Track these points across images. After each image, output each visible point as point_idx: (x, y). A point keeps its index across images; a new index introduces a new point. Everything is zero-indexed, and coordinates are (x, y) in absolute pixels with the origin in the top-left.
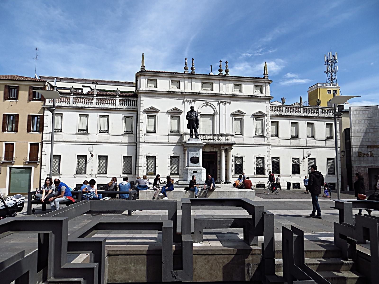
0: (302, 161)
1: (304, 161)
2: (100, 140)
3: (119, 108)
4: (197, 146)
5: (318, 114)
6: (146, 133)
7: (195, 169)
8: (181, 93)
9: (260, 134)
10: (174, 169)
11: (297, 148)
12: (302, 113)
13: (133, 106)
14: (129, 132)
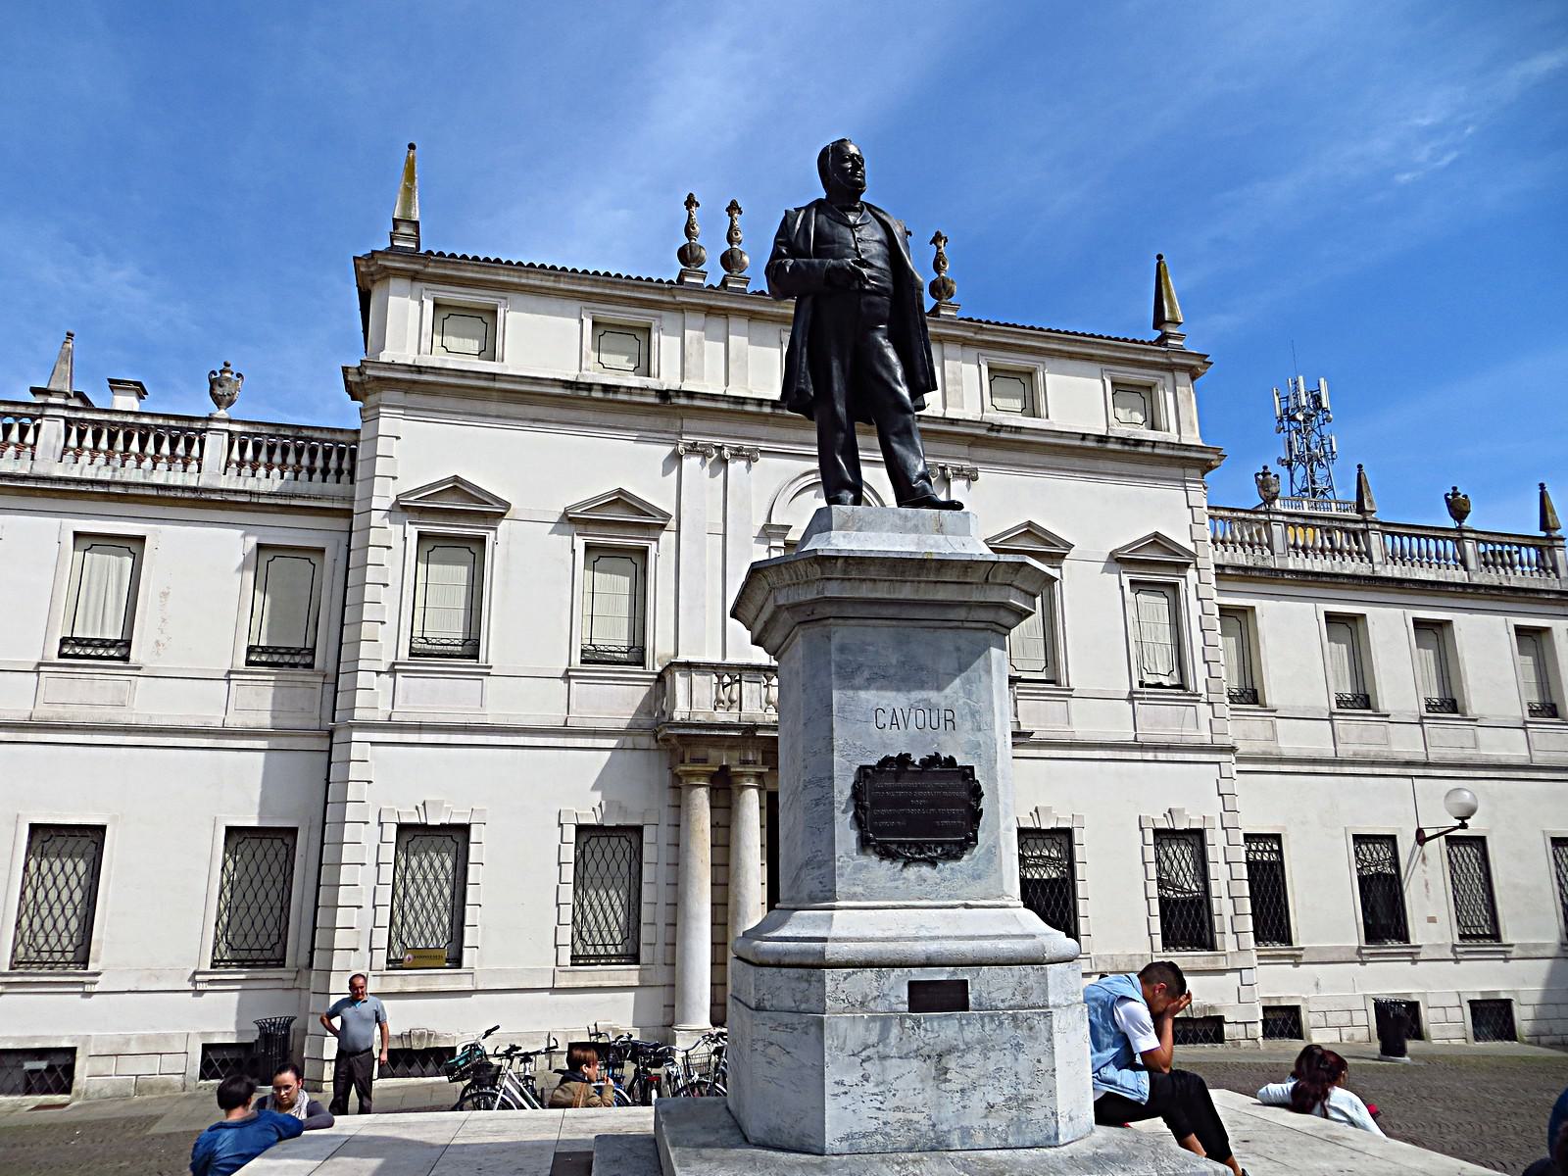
0: (1413, 852)
1: (1424, 859)
2: (60, 709)
3: (222, 485)
4: (942, 594)
5: (1466, 569)
6: (404, 654)
7: (933, 947)
8: (657, 401)
9: (1166, 682)
10: (601, 918)
11: (1338, 770)
12: (1380, 563)
13: (324, 480)
14: (287, 658)
